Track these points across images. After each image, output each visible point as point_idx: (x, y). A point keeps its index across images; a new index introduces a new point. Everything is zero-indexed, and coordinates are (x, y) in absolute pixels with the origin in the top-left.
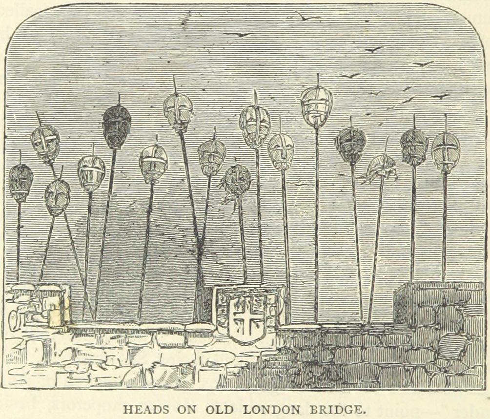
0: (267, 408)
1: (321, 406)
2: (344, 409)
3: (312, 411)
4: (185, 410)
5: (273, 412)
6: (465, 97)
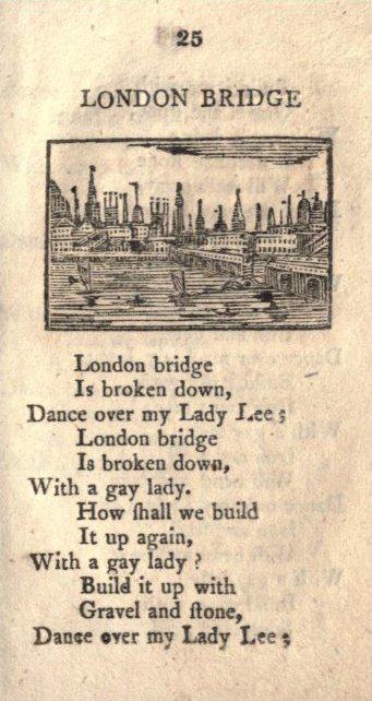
0: (126, 94)
1: (222, 91)
2: (152, 99)
3: (205, 100)
4: (167, 97)
5: (135, 103)
6: (97, 324)
